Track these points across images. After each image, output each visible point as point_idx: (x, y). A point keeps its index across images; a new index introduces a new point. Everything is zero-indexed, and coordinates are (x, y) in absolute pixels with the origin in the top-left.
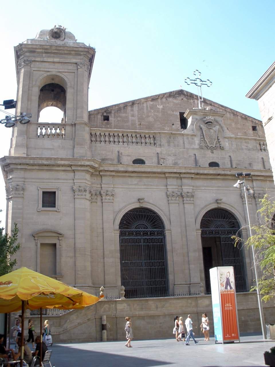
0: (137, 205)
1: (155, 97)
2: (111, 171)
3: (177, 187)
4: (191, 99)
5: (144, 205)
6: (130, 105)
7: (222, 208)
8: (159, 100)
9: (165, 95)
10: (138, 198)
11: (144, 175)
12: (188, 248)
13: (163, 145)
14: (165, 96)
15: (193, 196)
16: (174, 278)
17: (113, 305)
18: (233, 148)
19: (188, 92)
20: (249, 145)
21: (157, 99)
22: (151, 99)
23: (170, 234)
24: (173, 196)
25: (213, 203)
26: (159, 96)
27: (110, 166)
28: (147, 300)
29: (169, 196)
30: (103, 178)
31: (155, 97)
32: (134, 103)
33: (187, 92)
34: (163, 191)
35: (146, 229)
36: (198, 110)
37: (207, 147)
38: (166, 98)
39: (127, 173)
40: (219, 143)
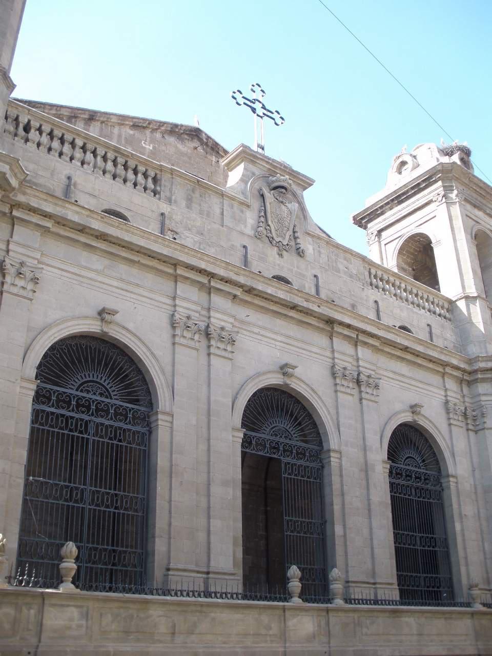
0: (92, 325)
1: (141, 121)
2: (45, 216)
3: (199, 309)
4: (213, 155)
5: (112, 331)
6: (85, 119)
7: (293, 389)
8: (148, 132)
9: (163, 126)
10: (100, 308)
11: (124, 254)
12: (209, 472)
13: (176, 202)
14: (163, 128)
15: (234, 341)
16: (169, 551)
17: (30, 608)
18: (321, 262)
19: (211, 138)
20: (351, 266)
21: (144, 128)
22: (131, 124)
23: (169, 424)
24: (189, 327)
25: (273, 372)
26: (149, 124)
27: (46, 200)
28: (147, 602)
29: (177, 323)
30: (16, 226)
31: (141, 121)
32: (93, 116)
33: (208, 137)
34: (163, 310)
35: (107, 397)
36: (260, 154)
37: (271, 240)
38: (163, 133)
39: (83, 233)
40: (295, 241)
